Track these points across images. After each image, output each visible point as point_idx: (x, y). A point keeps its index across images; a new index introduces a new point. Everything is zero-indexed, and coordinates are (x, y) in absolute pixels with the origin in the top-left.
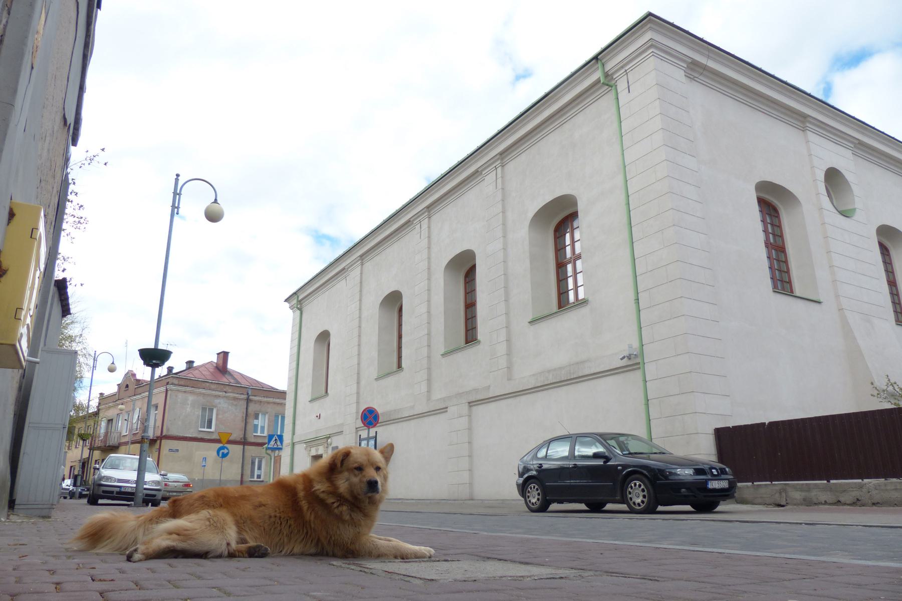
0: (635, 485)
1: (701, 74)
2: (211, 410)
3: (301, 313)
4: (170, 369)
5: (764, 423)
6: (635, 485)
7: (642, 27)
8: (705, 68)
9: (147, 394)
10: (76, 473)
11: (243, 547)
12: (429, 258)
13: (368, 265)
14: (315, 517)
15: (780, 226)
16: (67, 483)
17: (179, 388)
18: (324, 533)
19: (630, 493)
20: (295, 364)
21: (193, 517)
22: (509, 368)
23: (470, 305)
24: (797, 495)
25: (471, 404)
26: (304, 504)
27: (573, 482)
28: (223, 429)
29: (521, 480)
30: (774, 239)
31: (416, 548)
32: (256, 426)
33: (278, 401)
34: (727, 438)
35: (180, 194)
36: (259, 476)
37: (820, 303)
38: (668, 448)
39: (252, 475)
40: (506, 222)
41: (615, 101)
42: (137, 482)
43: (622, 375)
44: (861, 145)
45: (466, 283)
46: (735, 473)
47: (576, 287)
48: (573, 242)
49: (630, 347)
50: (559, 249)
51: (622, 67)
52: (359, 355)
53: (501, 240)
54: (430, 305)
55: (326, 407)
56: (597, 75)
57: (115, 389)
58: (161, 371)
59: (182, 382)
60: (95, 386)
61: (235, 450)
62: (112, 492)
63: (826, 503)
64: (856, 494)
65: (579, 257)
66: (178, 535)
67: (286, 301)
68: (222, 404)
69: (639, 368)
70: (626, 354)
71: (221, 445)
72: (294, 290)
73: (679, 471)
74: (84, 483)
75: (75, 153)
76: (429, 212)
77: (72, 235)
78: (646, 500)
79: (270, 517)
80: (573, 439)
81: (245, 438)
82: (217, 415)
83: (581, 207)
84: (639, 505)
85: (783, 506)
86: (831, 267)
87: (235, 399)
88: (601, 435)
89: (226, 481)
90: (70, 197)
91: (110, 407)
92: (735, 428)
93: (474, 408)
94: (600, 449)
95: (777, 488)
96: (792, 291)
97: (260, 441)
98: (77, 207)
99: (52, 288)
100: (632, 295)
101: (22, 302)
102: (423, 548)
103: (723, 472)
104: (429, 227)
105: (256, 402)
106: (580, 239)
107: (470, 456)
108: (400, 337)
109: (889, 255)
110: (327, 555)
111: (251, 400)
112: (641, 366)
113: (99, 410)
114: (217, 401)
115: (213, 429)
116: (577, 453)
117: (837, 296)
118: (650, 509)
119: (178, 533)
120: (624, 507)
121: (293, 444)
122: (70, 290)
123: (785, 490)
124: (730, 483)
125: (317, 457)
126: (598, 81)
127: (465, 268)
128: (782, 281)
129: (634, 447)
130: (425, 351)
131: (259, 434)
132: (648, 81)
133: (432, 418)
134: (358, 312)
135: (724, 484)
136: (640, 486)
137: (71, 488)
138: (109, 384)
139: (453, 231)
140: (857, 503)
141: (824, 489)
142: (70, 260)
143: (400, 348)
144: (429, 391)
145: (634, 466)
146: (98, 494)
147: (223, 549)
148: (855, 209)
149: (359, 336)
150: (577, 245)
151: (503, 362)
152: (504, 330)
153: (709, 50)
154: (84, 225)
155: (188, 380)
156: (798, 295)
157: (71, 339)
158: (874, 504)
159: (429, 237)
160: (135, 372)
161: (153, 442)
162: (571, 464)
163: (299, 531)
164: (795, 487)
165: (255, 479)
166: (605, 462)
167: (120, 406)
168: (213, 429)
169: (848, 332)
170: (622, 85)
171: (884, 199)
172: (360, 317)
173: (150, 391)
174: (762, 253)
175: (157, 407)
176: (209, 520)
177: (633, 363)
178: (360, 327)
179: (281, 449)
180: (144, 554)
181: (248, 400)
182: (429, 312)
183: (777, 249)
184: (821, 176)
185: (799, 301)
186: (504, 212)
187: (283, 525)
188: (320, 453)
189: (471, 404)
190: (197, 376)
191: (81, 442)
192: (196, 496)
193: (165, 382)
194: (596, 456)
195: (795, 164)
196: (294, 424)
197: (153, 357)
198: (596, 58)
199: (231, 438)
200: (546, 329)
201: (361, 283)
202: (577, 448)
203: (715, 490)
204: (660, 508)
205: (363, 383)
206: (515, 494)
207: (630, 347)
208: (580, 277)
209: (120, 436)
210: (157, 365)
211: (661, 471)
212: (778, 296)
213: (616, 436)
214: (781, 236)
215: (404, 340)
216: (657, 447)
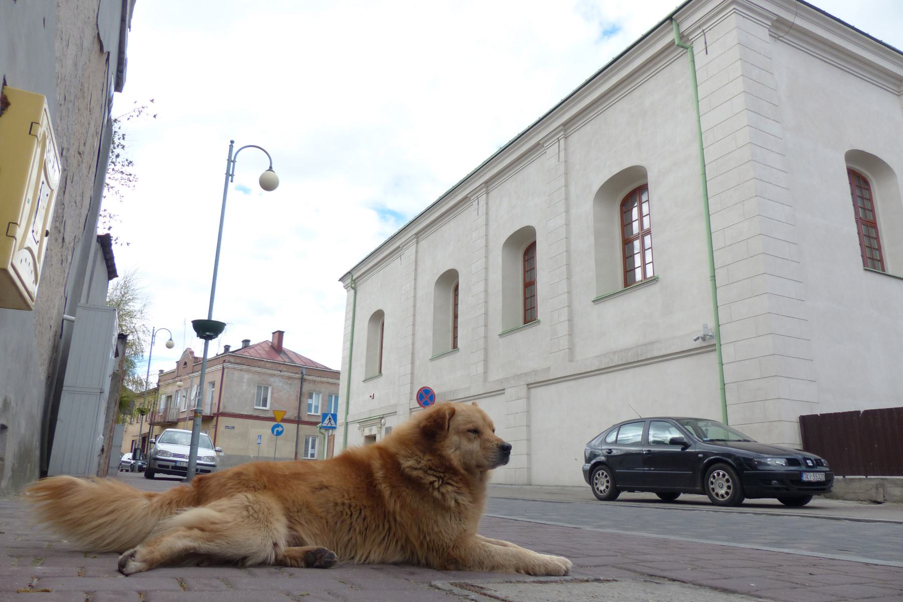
0: (718, 474)
2: (266, 389)
3: (356, 293)
4: (227, 348)
6: (718, 474)
8: (791, 26)
11: (297, 550)
13: (424, 243)
14: (401, 507)
15: (870, 200)
16: (127, 457)
17: (236, 366)
18: (415, 531)
19: (712, 483)
20: (348, 343)
21: (224, 502)
22: (571, 349)
23: (529, 285)
25: (530, 386)
26: (385, 489)
28: (277, 407)
29: (588, 466)
31: (547, 557)
32: (310, 405)
33: (331, 381)
34: (813, 427)
35: (234, 162)
36: (312, 455)
38: (748, 434)
39: (306, 454)
41: (690, 65)
42: (190, 457)
45: (525, 261)
46: (830, 465)
47: (644, 264)
48: (641, 216)
49: (705, 327)
50: (626, 224)
51: (699, 27)
52: (413, 335)
53: (564, 215)
54: (487, 284)
55: (379, 387)
56: (672, 36)
57: (174, 366)
58: (216, 347)
59: (238, 361)
61: (290, 428)
62: (167, 467)
65: (648, 232)
66: (202, 530)
67: (340, 280)
68: (277, 382)
69: (715, 350)
70: (701, 334)
71: (276, 423)
75: (121, 104)
76: (487, 187)
77: (121, 193)
78: (730, 491)
79: (336, 504)
80: (646, 423)
81: (299, 417)
82: (272, 393)
83: (652, 179)
84: (722, 496)
87: (290, 378)
89: (280, 459)
91: (169, 384)
92: (824, 417)
93: (533, 391)
94: (676, 434)
95: (873, 483)
96: (883, 270)
97: (314, 420)
98: (126, 163)
99: (94, 244)
100: (707, 272)
101: (16, 217)
102: (554, 557)
103: (818, 463)
104: (487, 204)
105: (310, 381)
106: (646, 213)
107: (528, 440)
108: (456, 317)
110: (418, 564)
111: (305, 380)
112: (717, 347)
114: (272, 380)
115: (268, 408)
116: (651, 439)
118: (735, 502)
119: (200, 527)
120: (704, 498)
121: (347, 424)
122: (115, 248)
123: (883, 486)
124: (827, 475)
125: (372, 438)
126: (672, 43)
127: (525, 246)
130: (482, 330)
135: (820, 477)
138: (168, 361)
139: (509, 209)
143: (455, 328)
144: (485, 373)
145: (717, 454)
146: (154, 468)
147: (268, 552)
149: (414, 315)
150: (646, 220)
151: (564, 343)
152: (566, 309)
156: (890, 273)
157: (130, 314)
159: (487, 214)
160: (193, 350)
161: (207, 419)
162: (645, 449)
163: (377, 526)
165: (309, 458)
166: (683, 449)
167: (178, 383)
168: (268, 408)
170: (698, 46)
172: (415, 296)
173: (202, 370)
176: (246, 508)
177: (709, 344)
178: (414, 306)
179: (335, 428)
180: (145, 561)
181: (302, 380)
182: (486, 291)
183: (867, 225)
185: (893, 281)
187: (355, 517)
188: (373, 433)
189: (530, 386)
190: (253, 354)
192: (230, 474)
194: (673, 442)
196: (348, 403)
197: (207, 329)
198: (670, 18)
199: (286, 417)
201: (416, 261)
202: (651, 432)
203: (810, 483)
204: (747, 501)
205: (417, 363)
206: (581, 480)
207: (705, 327)
208: (648, 254)
209: (179, 412)
210: (211, 338)
212: (870, 274)
213: (694, 422)
215: (460, 320)
216: (735, 433)
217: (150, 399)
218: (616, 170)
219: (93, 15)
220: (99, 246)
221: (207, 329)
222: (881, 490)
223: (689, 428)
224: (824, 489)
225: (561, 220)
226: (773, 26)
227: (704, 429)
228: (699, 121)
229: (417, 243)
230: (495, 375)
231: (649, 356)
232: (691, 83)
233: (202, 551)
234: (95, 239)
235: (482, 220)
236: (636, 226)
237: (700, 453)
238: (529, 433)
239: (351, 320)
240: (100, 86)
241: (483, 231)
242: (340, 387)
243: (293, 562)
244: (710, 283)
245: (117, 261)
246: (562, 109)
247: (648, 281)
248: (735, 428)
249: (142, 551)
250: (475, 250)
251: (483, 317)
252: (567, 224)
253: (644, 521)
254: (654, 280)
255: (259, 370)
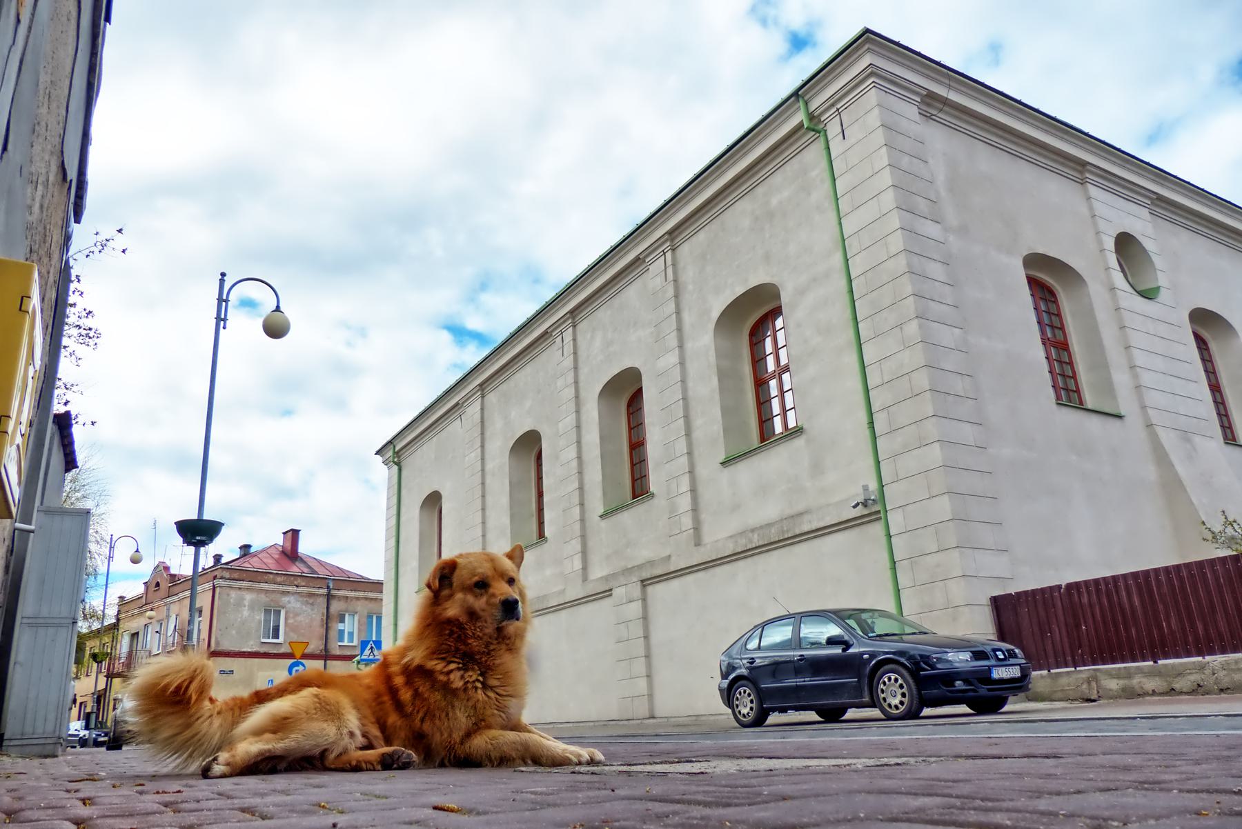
0: (890, 679)
1: (941, 110)
2: (278, 613)
3: (400, 470)
4: (218, 558)
5: (1059, 587)
6: (890, 679)
7: (857, 49)
8: (945, 102)
9: (188, 593)
10: (88, 710)
12: (576, 382)
13: (492, 398)
16: (76, 727)
19: (883, 691)
20: (393, 542)
22: (697, 529)
23: (637, 446)
24: (1113, 685)
25: (645, 583)
27: (800, 681)
28: (294, 637)
29: (725, 683)
30: (1054, 333)
32: (341, 632)
33: (371, 595)
34: (1005, 609)
35: (227, 301)
37: (1120, 417)
40: (680, 323)
41: (825, 152)
43: (857, 530)
44: (1160, 198)
45: (629, 414)
46: (1027, 656)
47: (784, 411)
49: (866, 488)
50: (758, 360)
51: (833, 105)
52: (484, 523)
53: (677, 351)
57: (141, 589)
60: (115, 582)
63: (1154, 693)
64: (1195, 677)
65: (786, 369)
68: (292, 602)
70: (861, 499)
72: (389, 438)
73: (951, 656)
74: (101, 725)
75: (81, 234)
78: (906, 700)
80: (799, 618)
81: (326, 649)
82: (286, 619)
83: (785, 299)
84: (897, 707)
85: (1094, 701)
86: (1133, 367)
87: (311, 595)
88: (835, 612)
90: (71, 300)
92: (1019, 594)
93: (650, 589)
94: (834, 630)
95: (1084, 676)
96: (1081, 403)
97: (348, 653)
98: (84, 314)
99: (51, 427)
103: (1012, 654)
104: (574, 340)
105: (339, 598)
106: (785, 339)
108: (540, 495)
109: (1207, 349)
111: (334, 597)
112: (882, 515)
113: (118, 620)
114: (285, 599)
115: (281, 640)
117: (1144, 408)
118: (912, 714)
122: (77, 431)
123: (1096, 679)
124: (1022, 669)
126: (801, 125)
127: (627, 393)
128: (1067, 390)
129: (881, 627)
131: (346, 643)
132: (865, 129)
133: (590, 606)
134: (479, 463)
135: (1015, 672)
136: (896, 680)
137: (83, 733)
139: (605, 346)
140: (1198, 690)
141: (1150, 674)
142: (74, 388)
148: (1158, 288)
149: (483, 496)
150: (783, 354)
151: (687, 522)
153: (949, 78)
154: (96, 340)
155: (240, 571)
156: (1089, 407)
158: (1222, 690)
159: (575, 353)
160: (168, 564)
162: (795, 654)
164: (1109, 674)
166: (844, 650)
167: (149, 613)
168: (281, 640)
169: (1161, 456)
170: (833, 129)
171: (1194, 272)
172: (483, 470)
173: (193, 589)
174: (1038, 353)
175: (200, 612)
177: (872, 511)
178: (483, 484)
180: (228, 764)
181: (329, 597)
182: (579, 457)
183: (1057, 345)
184: (1110, 244)
186: (678, 312)
190: (255, 565)
191: (95, 665)
193: (211, 576)
194: (832, 641)
195: (1079, 223)
197: (197, 532)
198: (796, 94)
199: (308, 651)
200: (743, 470)
201: (482, 422)
203: (1002, 681)
204: (927, 711)
207: (866, 488)
208: (788, 397)
210: (203, 543)
211: (925, 658)
212: (1065, 410)
213: (856, 613)
214: (1062, 328)
217: (106, 639)
218: (740, 290)
219: (58, 147)
220: (55, 428)
221: (197, 532)
222: (1094, 684)
223: (852, 623)
224: (1020, 687)
225: (673, 358)
226: (922, 102)
227: (869, 621)
228: (840, 224)
229: (483, 397)
230: (598, 571)
231: (798, 532)
232: (827, 175)
233: (278, 753)
234: (51, 418)
235: (569, 362)
236: (770, 361)
237: (865, 653)
238: (648, 647)
239: (395, 507)
240: (60, 223)
241: (570, 378)
242: (384, 602)
243: (369, 766)
244: (868, 432)
245: (78, 446)
246: (667, 212)
247: (793, 433)
248: (910, 618)
249: (223, 756)
250: (560, 401)
251: (577, 492)
252: (682, 363)
253: (801, 749)
254: (798, 431)
255: (263, 585)
